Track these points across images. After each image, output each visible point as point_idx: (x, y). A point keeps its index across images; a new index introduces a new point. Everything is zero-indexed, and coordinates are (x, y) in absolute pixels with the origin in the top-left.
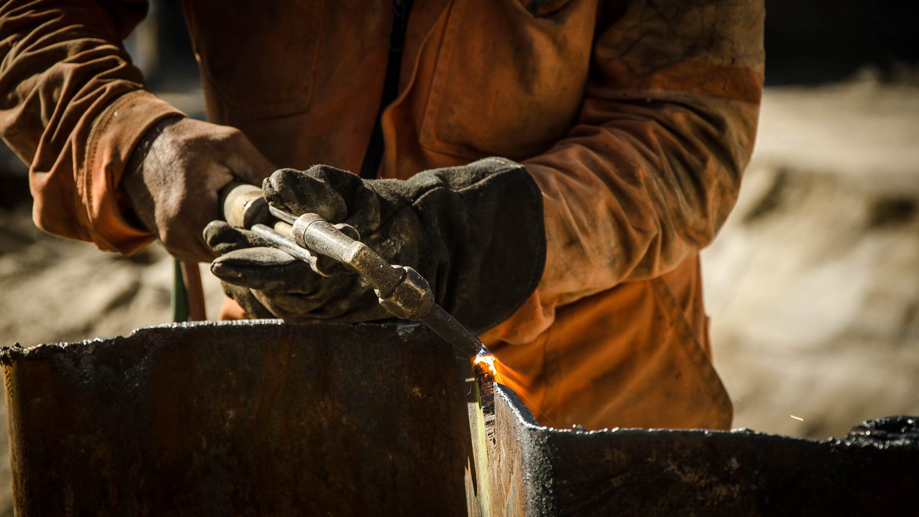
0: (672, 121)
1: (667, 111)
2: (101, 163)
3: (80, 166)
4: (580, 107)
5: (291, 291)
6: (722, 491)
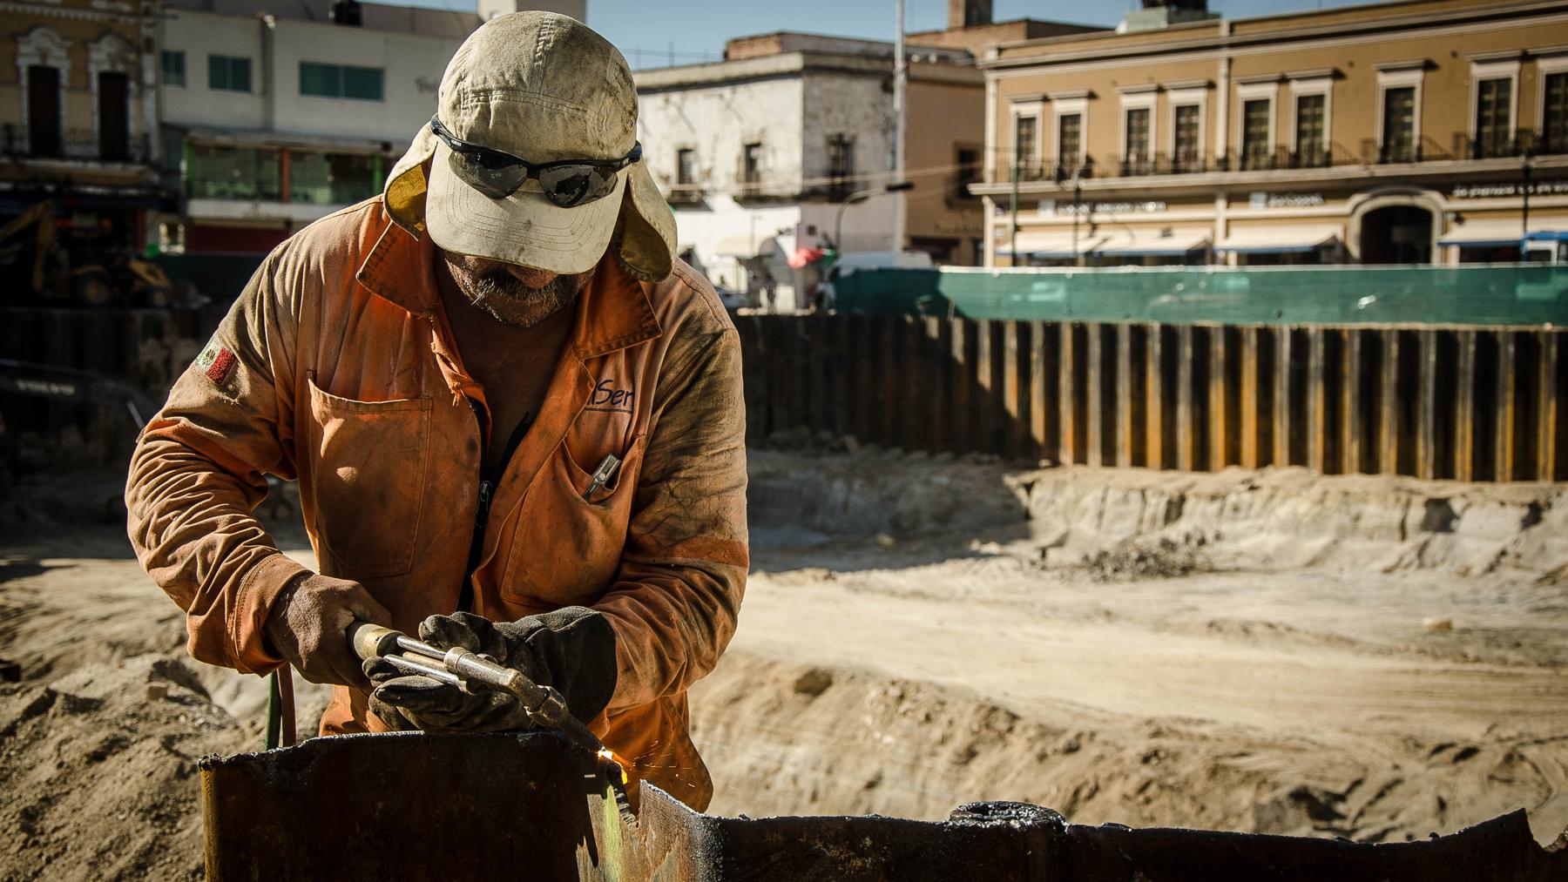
0: (691, 580)
1: (687, 573)
2: (250, 609)
3: (231, 611)
4: (618, 569)
5: (438, 710)
6: (858, 863)
